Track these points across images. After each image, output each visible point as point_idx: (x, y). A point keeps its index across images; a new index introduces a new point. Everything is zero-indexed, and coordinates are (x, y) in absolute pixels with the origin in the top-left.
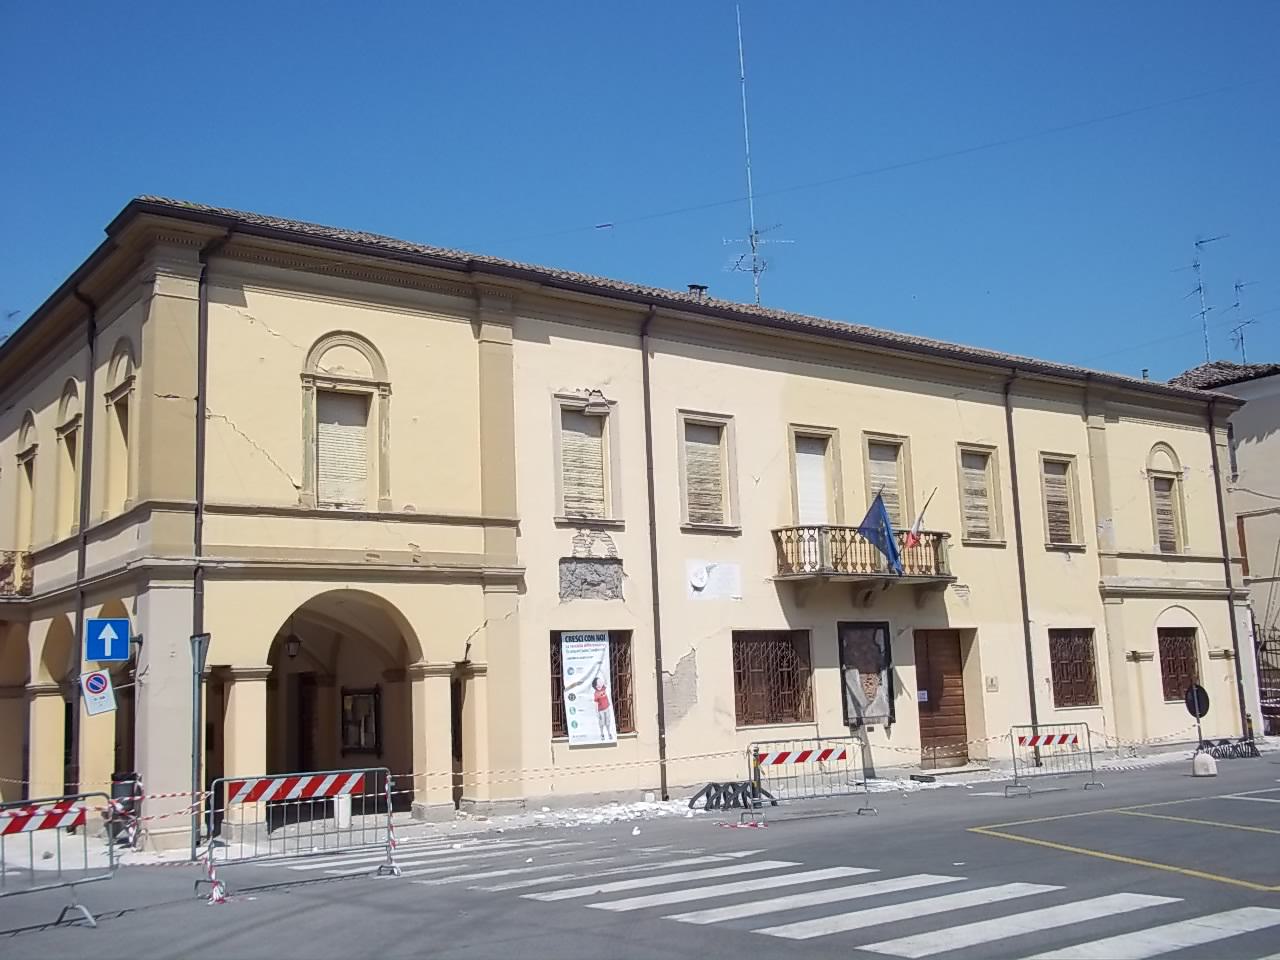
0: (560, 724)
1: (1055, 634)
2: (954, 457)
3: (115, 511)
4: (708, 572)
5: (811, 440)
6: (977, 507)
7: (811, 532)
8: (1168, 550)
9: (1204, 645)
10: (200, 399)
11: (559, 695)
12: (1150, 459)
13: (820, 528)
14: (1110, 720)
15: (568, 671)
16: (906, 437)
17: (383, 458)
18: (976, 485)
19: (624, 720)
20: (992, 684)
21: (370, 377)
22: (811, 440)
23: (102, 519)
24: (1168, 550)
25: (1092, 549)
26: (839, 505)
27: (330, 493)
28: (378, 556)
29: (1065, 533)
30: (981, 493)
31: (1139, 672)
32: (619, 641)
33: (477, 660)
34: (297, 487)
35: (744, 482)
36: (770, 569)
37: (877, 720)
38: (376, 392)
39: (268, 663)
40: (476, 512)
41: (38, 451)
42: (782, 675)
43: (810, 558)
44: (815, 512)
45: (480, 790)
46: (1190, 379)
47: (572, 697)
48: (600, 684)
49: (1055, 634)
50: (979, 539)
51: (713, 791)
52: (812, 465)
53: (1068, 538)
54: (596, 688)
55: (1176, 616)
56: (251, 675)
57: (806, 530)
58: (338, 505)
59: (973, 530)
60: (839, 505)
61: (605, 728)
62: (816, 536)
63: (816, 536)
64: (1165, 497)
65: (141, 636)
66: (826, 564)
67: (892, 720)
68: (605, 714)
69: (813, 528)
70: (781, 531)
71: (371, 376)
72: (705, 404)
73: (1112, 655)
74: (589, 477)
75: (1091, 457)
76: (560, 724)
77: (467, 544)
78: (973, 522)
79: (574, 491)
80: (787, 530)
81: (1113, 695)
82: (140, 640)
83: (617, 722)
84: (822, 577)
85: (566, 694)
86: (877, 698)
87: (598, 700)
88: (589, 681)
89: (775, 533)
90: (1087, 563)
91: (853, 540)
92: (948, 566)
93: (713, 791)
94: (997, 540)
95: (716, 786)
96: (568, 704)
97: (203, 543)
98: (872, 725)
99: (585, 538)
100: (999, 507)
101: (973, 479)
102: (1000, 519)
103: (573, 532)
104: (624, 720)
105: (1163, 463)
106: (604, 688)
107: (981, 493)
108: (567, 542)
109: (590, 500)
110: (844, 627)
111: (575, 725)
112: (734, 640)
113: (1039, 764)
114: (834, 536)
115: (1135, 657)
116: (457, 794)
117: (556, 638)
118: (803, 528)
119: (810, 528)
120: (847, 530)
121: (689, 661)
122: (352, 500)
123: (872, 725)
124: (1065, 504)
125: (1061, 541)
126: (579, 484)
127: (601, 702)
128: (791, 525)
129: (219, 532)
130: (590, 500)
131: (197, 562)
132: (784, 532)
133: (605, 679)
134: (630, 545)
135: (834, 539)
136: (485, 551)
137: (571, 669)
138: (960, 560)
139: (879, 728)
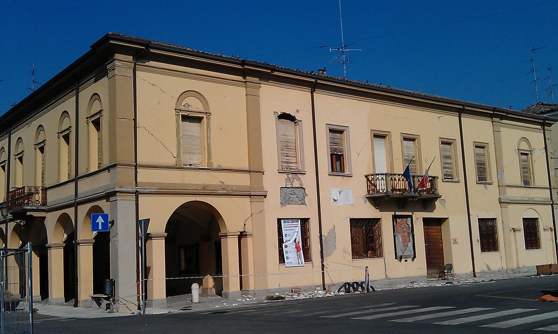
0: (282, 259)
1: (481, 221)
2: (437, 143)
3: (94, 168)
4: (340, 193)
5: (379, 136)
6: (447, 163)
7: (382, 176)
8: (527, 183)
9: (541, 226)
10: (135, 120)
11: (281, 246)
12: (519, 144)
13: (386, 174)
14: (504, 258)
15: (285, 236)
16: (390, 132)
17: (209, 145)
18: (447, 154)
19: (307, 258)
20: (455, 242)
21: (202, 110)
22: (379, 136)
23: (87, 172)
24: (527, 183)
25: (495, 184)
26: (391, 165)
27: (186, 159)
28: (208, 187)
29: (485, 177)
30: (449, 157)
31: (515, 235)
32: (304, 222)
33: (249, 230)
34: (175, 157)
35: (354, 155)
36: (364, 192)
37: (407, 257)
38: (205, 116)
39: (165, 232)
40: (247, 168)
41: (46, 142)
42: (370, 238)
43: (381, 186)
44: (382, 168)
45: (252, 285)
46: (531, 110)
47: (286, 246)
48: (402, 249)
49: (481, 221)
50: (448, 177)
51: (347, 286)
52: (380, 145)
53: (485, 179)
54: (295, 243)
55: (531, 214)
56: (158, 237)
57: (380, 175)
58: (190, 165)
59: (446, 173)
60: (391, 165)
61: (299, 259)
62: (384, 178)
63: (384, 178)
64: (336, 150)
65: (113, 221)
66: (388, 190)
67: (415, 257)
68: (299, 253)
69: (383, 174)
70: (369, 176)
71: (203, 110)
72: (337, 122)
73: (504, 230)
74: (291, 153)
75: (495, 144)
76: (282, 259)
77: (243, 180)
78: (446, 170)
79: (285, 159)
80: (371, 176)
81: (505, 246)
82: (112, 223)
83: (304, 257)
84: (387, 195)
85: (284, 245)
86: (408, 247)
87: (296, 248)
88: (293, 240)
89: (366, 176)
90: (493, 189)
91: (399, 180)
92: (438, 191)
93: (347, 286)
94: (456, 180)
95: (348, 283)
96: (285, 249)
97: (138, 181)
98: (406, 259)
99: (290, 179)
100: (457, 166)
101: (446, 151)
102: (457, 171)
103: (285, 176)
104: (307, 258)
105: (524, 146)
106: (299, 242)
107: (449, 157)
108: (281, 181)
109: (291, 163)
110: (395, 217)
111: (287, 258)
112: (350, 222)
113: (475, 276)
114: (391, 178)
115: (514, 230)
116: (241, 287)
117: (279, 220)
118: (378, 175)
119: (381, 174)
120: (420, 177)
121: (333, 231)
122: (197, 162)
123: (406, 259)
124: (484, 164)
125: (482, 178)
126: (287, 156)
127: (297, 248)
128: (372, 173)
129: (144, 176)
130: (291, 163)
131: (136, 190)
132: (370, 176)
133: (299, 239)
134: (308, 181)
135: (391, 179)
136: (251, 184)
137: (286, 234)
138: (442, 188)
139: (409, 260)
